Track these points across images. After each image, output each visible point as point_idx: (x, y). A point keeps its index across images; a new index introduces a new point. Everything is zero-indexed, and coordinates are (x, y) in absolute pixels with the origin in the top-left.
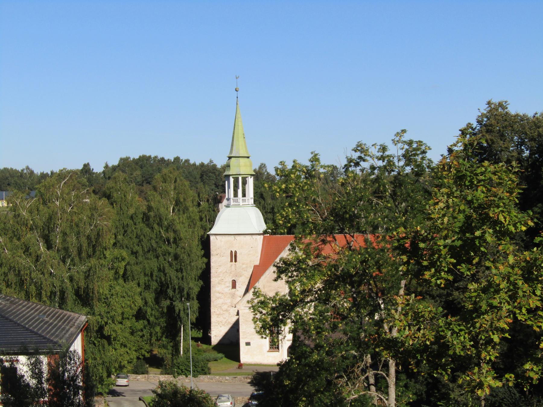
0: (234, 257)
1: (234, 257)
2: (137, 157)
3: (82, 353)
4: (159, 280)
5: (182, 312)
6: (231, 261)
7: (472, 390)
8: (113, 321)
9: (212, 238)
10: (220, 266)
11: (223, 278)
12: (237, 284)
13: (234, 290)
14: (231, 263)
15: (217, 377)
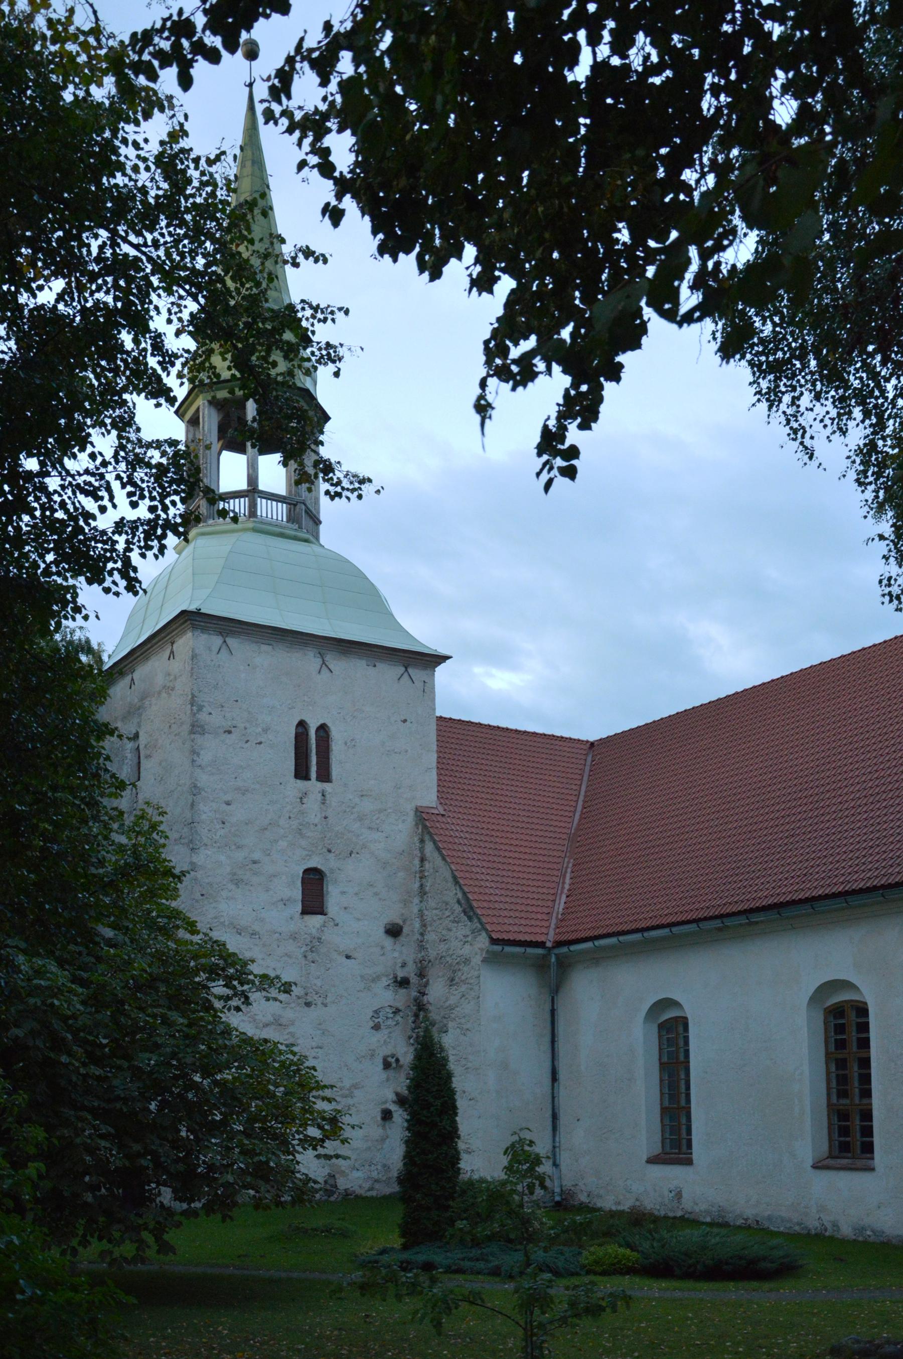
3: (832, 1005)
6: (301, 773)
7: (322, 471)
10: (244, 791)
11: (256, 856)
12: (297, 893)
13: (315, 921)
14: (300, 784)
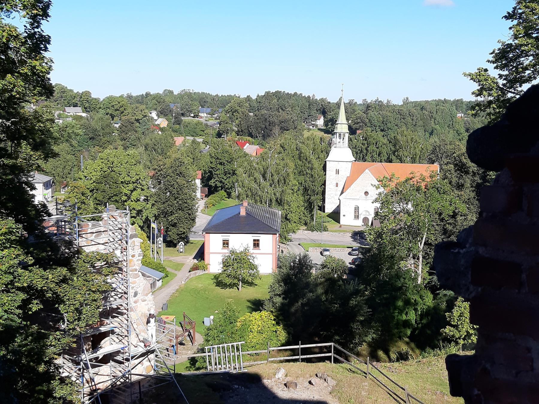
0: (338, 172)
1: (338, 172)
2: (274, 91)
4: (305, 186)
6: (336, 174)
8: (291, 213)
9: (327, 162)
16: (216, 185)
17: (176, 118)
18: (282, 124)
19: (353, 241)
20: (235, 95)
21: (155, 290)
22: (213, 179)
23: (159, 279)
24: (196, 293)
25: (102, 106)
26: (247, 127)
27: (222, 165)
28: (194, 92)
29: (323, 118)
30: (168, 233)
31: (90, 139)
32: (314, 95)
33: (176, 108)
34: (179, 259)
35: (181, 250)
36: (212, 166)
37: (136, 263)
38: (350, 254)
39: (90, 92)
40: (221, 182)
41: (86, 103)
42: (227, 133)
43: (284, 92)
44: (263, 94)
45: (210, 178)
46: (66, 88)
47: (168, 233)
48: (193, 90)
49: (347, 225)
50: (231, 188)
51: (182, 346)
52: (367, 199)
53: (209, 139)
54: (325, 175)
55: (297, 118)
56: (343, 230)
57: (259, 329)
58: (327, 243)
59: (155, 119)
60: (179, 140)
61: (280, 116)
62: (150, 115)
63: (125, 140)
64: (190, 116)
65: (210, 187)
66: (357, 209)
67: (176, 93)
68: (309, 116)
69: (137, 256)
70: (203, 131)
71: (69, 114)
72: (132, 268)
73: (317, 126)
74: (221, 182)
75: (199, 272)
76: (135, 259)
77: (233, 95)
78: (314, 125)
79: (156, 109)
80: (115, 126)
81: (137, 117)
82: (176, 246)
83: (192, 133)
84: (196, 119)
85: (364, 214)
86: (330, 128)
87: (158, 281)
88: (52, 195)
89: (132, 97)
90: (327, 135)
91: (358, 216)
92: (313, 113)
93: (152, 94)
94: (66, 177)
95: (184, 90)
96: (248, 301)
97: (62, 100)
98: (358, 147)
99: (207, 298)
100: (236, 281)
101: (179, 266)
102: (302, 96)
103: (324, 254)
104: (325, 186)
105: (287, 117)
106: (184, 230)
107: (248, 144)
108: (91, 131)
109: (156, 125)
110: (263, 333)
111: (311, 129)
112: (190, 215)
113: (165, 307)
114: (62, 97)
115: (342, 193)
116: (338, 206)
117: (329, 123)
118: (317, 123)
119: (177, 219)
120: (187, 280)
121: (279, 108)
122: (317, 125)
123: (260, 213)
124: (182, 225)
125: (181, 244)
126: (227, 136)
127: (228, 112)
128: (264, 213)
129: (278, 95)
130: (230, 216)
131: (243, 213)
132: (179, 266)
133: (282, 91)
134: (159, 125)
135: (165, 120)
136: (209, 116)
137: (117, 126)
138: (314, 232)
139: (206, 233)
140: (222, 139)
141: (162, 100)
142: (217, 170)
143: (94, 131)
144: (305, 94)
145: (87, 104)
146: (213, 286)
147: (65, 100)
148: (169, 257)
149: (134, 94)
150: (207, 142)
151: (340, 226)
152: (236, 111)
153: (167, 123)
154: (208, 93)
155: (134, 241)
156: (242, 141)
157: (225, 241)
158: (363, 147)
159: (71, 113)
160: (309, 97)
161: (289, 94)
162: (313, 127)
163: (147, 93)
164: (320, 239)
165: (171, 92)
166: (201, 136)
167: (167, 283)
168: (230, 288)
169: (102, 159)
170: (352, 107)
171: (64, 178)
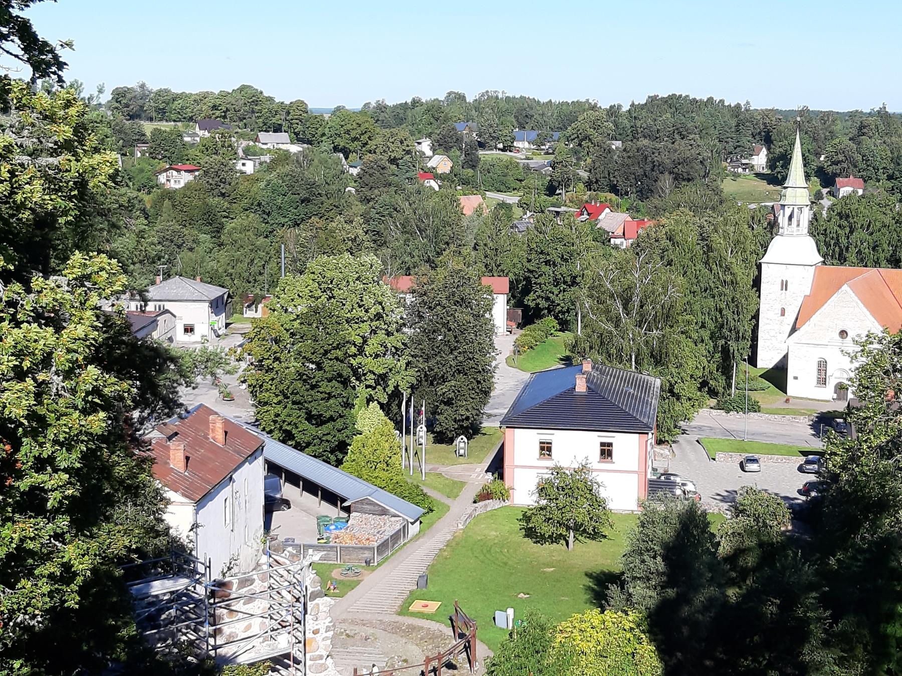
0: (785, 286)
1: (785, 286)
2: (666, 96)
5: (736, 352)
6: (782, 290)
9: (763, 265)
15: (767, 415)
16: (537, 304)
17: (468, 154)
18: (679, 167)
19: (813, 435)
20: (588, 100)
21: (406, 541)
22: (532, 293)
23: (413, 521)
24: (485, 551)
25: (327, 131)
26: (607, 173)
27: (550, 265)
28: (507, 95)
29: (766, 152)
30: (437, 417)
31: (303, 202)
32: (748, 103)
33: (468, 133)
34: (455, 470)
35: (462, 452)
36: (531, 268)
37: (321, 644)
38: (801, 469)
39: (305, 102)
40: (547, 299)
41: (298, 124)
42: (567, 186)
43: (688, 96)
44: (643, 102)
45: (527, 291)
46: (261, 93)
47: (437, 417)
48: (503, 92)
49: (802, 398)
50: (568, 311)
51: (450, 671)
52: (844, 345)
53: (532, 198)
54: (759, 297)
55: (710, 155)
56: (792, 409)
57: (598, 648)
58: (759, 439)
59: (427, 155)
60: (470, 203)
61: (675, 151)
62: (418, 148)
63: (369, 201)
64: (496, 148)
65: (526, 309)
66: (822, 366)
67: (470, 99)
68: (735, 148)
69: (322, 631)
70: (521, 181)
71: (265, 147)
72: (314, 654)
73: (752, 167)
74: (547, 299)
75: (493, 504)
76: (319, 637)
77: (584, 100)
78: (746, 166)
79: (429, 136)
80: (350, 172)
81: (392, 154)
82: (453, 442)
83: (497, 185)
84: (508, 153)
85: (838, 376)
86: (779, 172)
87: (413, 523)
88: (228, 321)
89: (386, 107)
90: (774, 188)
91: (825, 379)
92: (744, 141)
93: (424, 101)
94: (255, 280)
95: (487, 92)
96: (586, 575)
97: (254, 118)
98: (830, 232)
99: (506, 564)
100: (563, 531)
101: (455, 488)
102: (723, 105)
103: (747, 468)
104: (758, 321)
105: (688, 154)
106: (468, 414)
107: (607, 210)
108: (304, 187)
109: (429, 169)
110: (606, 657)
111: (739, 175)
112: (479, 382)
113: (423, 581)
114: (253, 112)
115: (794, 330)
116: (784, 357)
117: (778, 164)
118: (753, 163)
119: (454, 392)
120: (469, 521)
121: (674, 132)
122: (753, 166)
123: (616, 386)
124: (464, 403)
125: (462, 439)
126: (567, 192)
127: (572, 140)
128: (624, 386)
129: (673, 103)
130: (557, 392)
131: (581, 386)
132: (455, 488)
133: (684, 95)
134: (434, 168)
135: (446, 159)
136: (532, 147)
137: (355, 171)
138: (731, 413)
139: (507, 427)
140: (556, 197)
141: (442, 115)
142: (541, 275)
143: (309, 187)
144: (731, 101)
145: (299, 126)
146: (519, 537)
147: (259, 117)
148: (437, 466)
149: (390, 103)
150: (527, 205)
151: (787, 401)
152: (587, 138)
153: (450, 164)
154: (531, 98)
155: (318, 605)
156: (596, 203)
157: (543, 443)
158: (840, 232)
159: (269, 145)
160: (738, 106)
161: (697, 102)
162: (744, 169)
163: (414, 99)
164: (742, 428)
165: (462, 98)
166: (516, 191)
167: (431, 525)
168: (552, 542)
169: (313, 273)
170: (830, 126)
171: (250, 282)
